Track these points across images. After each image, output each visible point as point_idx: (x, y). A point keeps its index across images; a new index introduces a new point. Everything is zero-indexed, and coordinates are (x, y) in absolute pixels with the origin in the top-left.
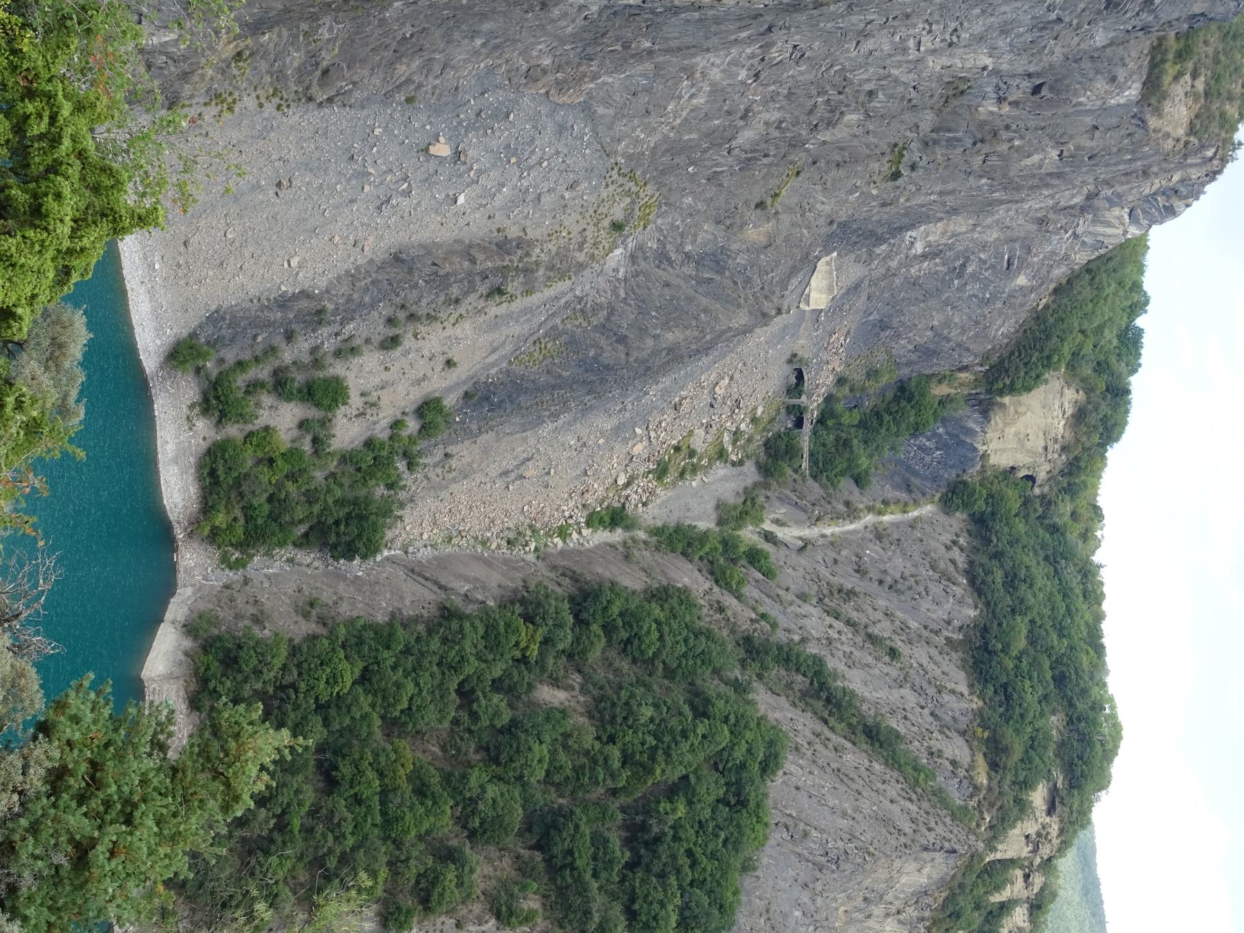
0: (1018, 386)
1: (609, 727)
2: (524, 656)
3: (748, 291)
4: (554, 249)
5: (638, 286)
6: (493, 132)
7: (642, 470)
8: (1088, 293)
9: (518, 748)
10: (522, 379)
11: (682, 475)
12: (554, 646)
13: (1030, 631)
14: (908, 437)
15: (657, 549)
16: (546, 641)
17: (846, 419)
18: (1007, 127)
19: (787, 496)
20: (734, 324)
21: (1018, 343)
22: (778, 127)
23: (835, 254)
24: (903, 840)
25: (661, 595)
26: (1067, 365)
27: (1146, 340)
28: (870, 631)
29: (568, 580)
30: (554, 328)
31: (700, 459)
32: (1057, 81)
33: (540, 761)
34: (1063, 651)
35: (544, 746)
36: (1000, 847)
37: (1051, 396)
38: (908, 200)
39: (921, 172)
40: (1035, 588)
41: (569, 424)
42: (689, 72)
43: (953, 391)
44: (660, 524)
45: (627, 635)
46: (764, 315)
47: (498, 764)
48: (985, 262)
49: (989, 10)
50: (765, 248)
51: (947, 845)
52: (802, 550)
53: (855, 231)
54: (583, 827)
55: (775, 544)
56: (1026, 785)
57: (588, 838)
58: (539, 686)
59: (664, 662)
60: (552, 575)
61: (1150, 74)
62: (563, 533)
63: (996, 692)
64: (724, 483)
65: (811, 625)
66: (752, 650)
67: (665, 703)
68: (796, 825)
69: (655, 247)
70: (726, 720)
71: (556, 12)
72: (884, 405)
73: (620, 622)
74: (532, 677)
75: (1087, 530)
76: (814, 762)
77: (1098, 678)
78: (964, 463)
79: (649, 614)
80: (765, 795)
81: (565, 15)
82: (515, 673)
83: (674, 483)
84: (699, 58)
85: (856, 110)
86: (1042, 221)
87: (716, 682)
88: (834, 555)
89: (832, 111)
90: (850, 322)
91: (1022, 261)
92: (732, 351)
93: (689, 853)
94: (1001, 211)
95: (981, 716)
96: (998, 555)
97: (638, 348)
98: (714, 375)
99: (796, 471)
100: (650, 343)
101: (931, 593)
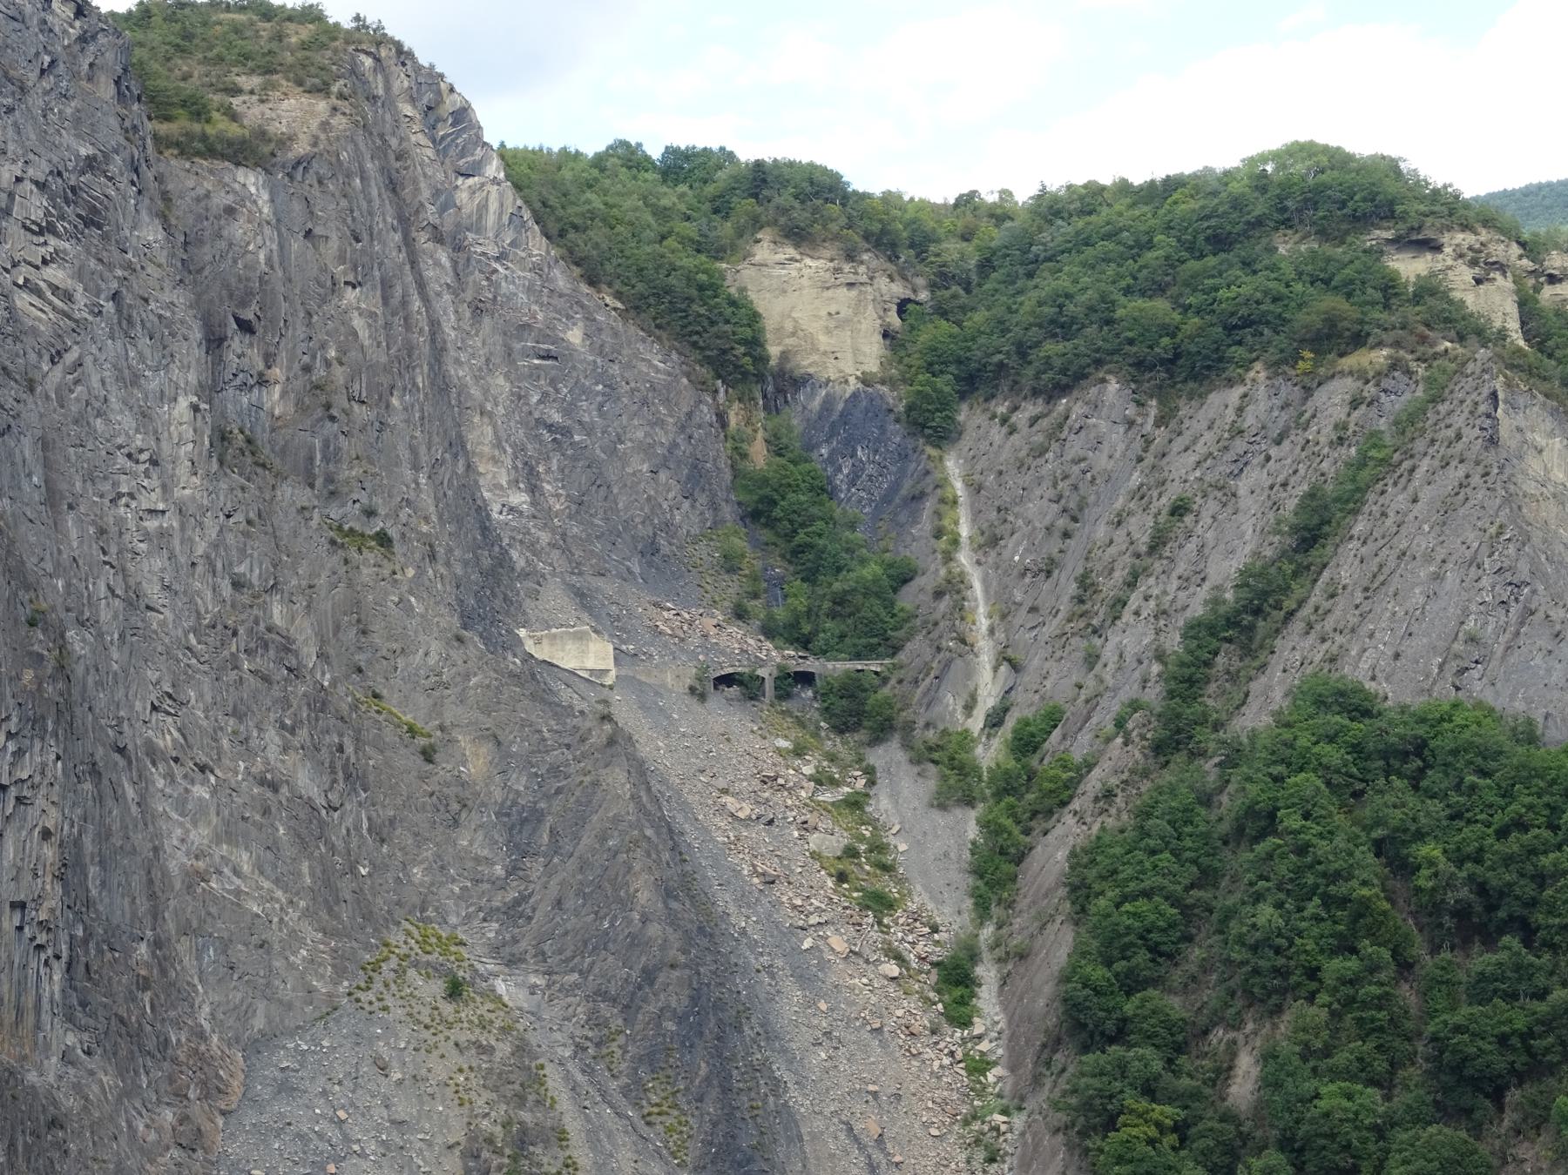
1: (1293, 979)
3: (572, 770)
4: (487, 1095)
7: (875, 935)
8: (598, 234)
9: (1325, 1136)
10: (711, 1144)
11: (886, 868)
12: (1157, 1077)
13: (1143, 293)
14: (834, 503)
15: (1010, 905)
16: (1149, 1090)
17: (801, 603)
18: (307, 369)
19: (925, 694)
21: (680, 337)
22: (292, 731)
23: (522, 633)
24: (1476, 480)
25: (1080, 892)
26: (716, 259)
27: (682, 143)
28: (1144, 549)
29: (1057, 1056)
30: (625, 1091)
31: (861, 838)
32: (231, 296)
33: (1349, 1097)
35: (1323, 1090)
36: (1498, 324)
37: (766, 282)
39: (378, 500)
40: (1072, 289)
41: (791, 1061)
42: (195, 878)
43: (760, 435)
44: (969, 903)
46: (611, 742)
48: (545, 395)
49: (97, 405)
50: (499, 743)
51: (1482, 408)
52: (1015, 667)
53: (479, 601)
54: (1457, 1019)
55: (1006, 710)
56: (1390, 288)
57: (1477, 1009)
58: (1230, 1100)
59: (1188, 889)
60: (1048, 1082)
61: (223, 157)
62: (978, 1067)
63: (1240, 343)
64: (902, 798)
65: (1136, 647)
66: (1173, 742)
67: (1251, 884)
68: (1456, 656)
69: (495, 925)
70: (1278, 779)
71: (70, 1103)
72: (780, 541)
73: (1120, 966)
75: (992, 216)
76: (1353, 630)
77: (1215, 184)
79: (1109, 916)
80: (1403, 709)
81: (78, 1088)
82: (1200, 1144)
83: (900, 881)
85: (265, 607)
86: (478, 310)
87: (1225, 799)
88: (1023, 611)
89: (266, 646)
90: (639, 603)
91: (543, 337)
92: (679, 793)
93: (1502, 833)
94: (459, 373)
95: (1277, 364)
96: (1022, 351)
99: (885, 681)
100: (654, 930)
101: (1082, 453)
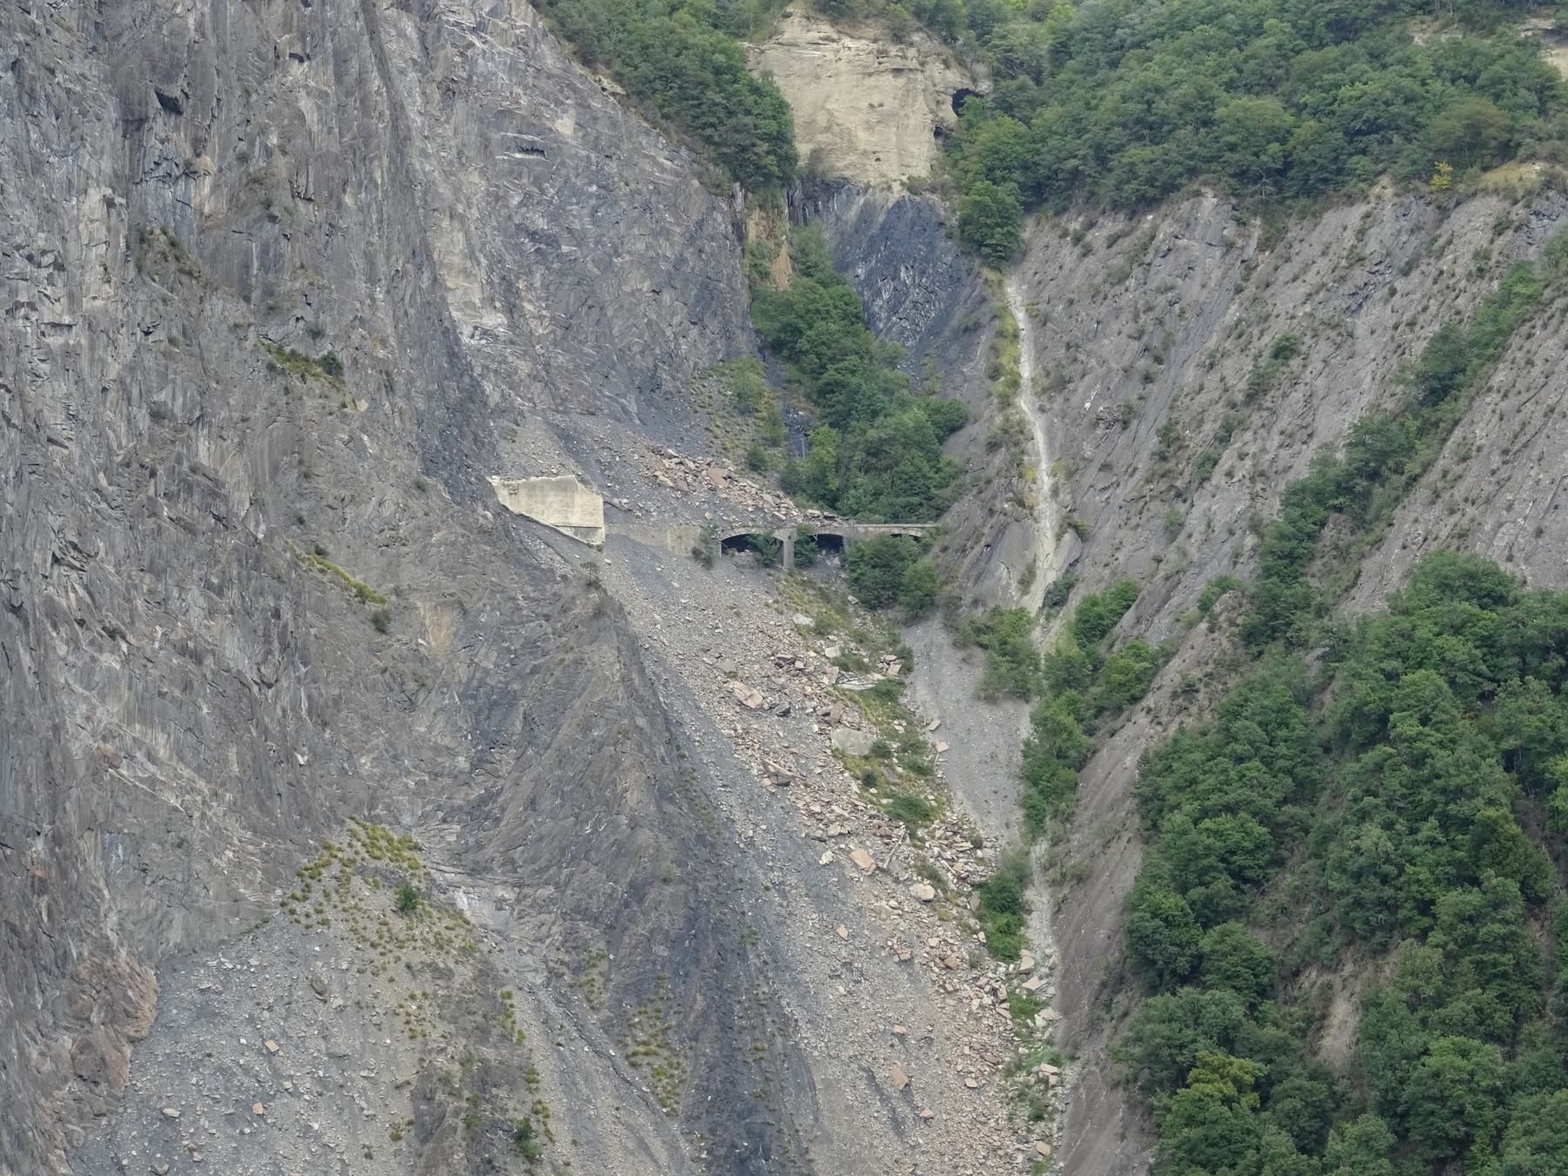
0: (772, 127)
2: (1256, 1087)
3: (551, 646)
4: (443, 1027)
5: (533, 860)
6: (199, 1149)
7: (906, 849)
10: (707, 1090)
11: (921, 771)
12: (1236, 1026)
13: (1248, 89)
14: (871, 335)
15: (1068, 818)
16: (1227, 1041)
17: (828, 453)
18: (243, 158)
19: (974, 565)
20: (615, 671)
21: (690, 129)
22: (220, 591)
23: (495, 481)
25: (1151, 806)
28: (1240, 397)
29: (1120, 997)
30: (607, 1026)
31: (893, 735)
32: (153, 69)
33: (1464, 1054)
34: (1287, 26)
35: (1433, 1045)
37: (796, 66)
38: (384, 342)
40: (1163, 82)
42: (101, 763)
43: (784, 250)
44: (1019, 814)
45: (1225, 876)
46: (599, 613)
47: (1467, 1141)
48: (528, 196)
50: (465, 612)
52: (1082, 534)
53: (444, 441)
55: (1070, 586)
60: (1107, 1029)
62: (1025, 1008)
63: (1364, 152)
65: (1227, 515)
66: (1268, 628)
67: (1356, 800)
69: (457, 828)
70: (1391, 676)
72: (805, 379)
73: (1196, 893)
74: (1298, 1069)
76: (1488, 501)
78: (925, 225)
79: (1185, 833)
80: (1545, 596)
83: (939, 787)
84: (76, 748)
85: (188, 443)
86: (449, 91)
90: (635, 449)
91: (527, 126)
94: (425, 167)
95: (1407, 178)
96: (1102, 155)
97: (655, 859)
98: (723, 709)
99: (926, 548)
100: (644, 837)
101: (1169, 281)
